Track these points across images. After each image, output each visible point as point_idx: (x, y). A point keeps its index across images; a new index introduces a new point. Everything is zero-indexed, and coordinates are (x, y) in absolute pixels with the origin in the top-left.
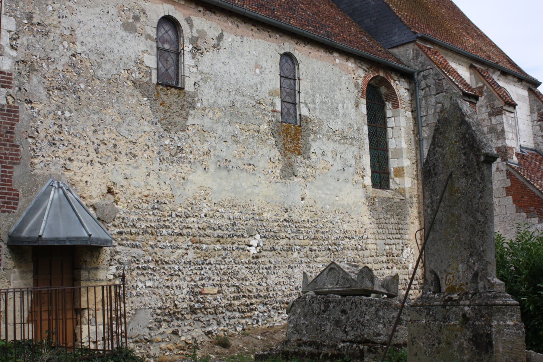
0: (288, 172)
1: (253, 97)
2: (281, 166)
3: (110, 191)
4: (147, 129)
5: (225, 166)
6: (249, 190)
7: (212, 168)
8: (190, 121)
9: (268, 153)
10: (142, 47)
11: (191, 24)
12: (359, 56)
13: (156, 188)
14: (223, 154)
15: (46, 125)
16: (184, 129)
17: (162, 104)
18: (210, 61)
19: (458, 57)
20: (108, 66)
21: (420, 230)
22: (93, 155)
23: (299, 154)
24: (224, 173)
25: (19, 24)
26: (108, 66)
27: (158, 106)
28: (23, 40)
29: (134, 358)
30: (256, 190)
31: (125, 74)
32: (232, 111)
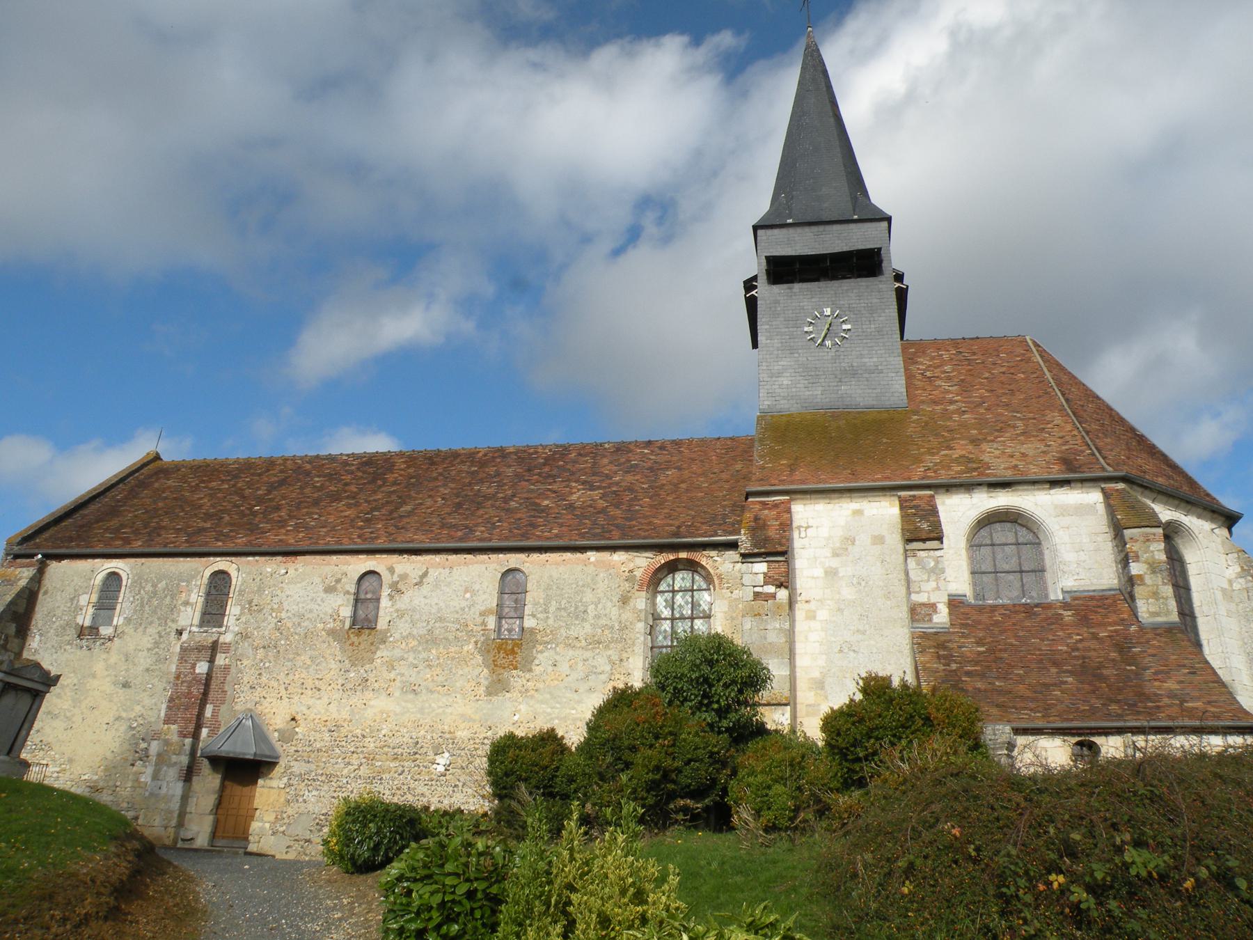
0: (491, 692)
1: (458, 621)
2: (486, 683)
3: (293, 719)
4: (333, 666)
5: (413, 690)
6: (440, 710)
7: (397, 694)
8: (379, 654)
9: (476, 671)
10: (340, 602)
11: (391, 570)
12: (1146, 488)
13: (335, 713)
14: (412, 679)
15: (248, 677)
16: (372, 661)
17: (352, 644)
18: (412, 598)
19: (1183, 505)
20: (306, 624)
21: (793, 731)
22: (283, 692)
23: (516, 668)
24: (411, 696)
25: (243, 608)
26: (306, 624)
27: (347, 647)
28: (243, 619)
29: (638, 694)
30: (449, 710)
31: (320, 626)
32: (430, 640)
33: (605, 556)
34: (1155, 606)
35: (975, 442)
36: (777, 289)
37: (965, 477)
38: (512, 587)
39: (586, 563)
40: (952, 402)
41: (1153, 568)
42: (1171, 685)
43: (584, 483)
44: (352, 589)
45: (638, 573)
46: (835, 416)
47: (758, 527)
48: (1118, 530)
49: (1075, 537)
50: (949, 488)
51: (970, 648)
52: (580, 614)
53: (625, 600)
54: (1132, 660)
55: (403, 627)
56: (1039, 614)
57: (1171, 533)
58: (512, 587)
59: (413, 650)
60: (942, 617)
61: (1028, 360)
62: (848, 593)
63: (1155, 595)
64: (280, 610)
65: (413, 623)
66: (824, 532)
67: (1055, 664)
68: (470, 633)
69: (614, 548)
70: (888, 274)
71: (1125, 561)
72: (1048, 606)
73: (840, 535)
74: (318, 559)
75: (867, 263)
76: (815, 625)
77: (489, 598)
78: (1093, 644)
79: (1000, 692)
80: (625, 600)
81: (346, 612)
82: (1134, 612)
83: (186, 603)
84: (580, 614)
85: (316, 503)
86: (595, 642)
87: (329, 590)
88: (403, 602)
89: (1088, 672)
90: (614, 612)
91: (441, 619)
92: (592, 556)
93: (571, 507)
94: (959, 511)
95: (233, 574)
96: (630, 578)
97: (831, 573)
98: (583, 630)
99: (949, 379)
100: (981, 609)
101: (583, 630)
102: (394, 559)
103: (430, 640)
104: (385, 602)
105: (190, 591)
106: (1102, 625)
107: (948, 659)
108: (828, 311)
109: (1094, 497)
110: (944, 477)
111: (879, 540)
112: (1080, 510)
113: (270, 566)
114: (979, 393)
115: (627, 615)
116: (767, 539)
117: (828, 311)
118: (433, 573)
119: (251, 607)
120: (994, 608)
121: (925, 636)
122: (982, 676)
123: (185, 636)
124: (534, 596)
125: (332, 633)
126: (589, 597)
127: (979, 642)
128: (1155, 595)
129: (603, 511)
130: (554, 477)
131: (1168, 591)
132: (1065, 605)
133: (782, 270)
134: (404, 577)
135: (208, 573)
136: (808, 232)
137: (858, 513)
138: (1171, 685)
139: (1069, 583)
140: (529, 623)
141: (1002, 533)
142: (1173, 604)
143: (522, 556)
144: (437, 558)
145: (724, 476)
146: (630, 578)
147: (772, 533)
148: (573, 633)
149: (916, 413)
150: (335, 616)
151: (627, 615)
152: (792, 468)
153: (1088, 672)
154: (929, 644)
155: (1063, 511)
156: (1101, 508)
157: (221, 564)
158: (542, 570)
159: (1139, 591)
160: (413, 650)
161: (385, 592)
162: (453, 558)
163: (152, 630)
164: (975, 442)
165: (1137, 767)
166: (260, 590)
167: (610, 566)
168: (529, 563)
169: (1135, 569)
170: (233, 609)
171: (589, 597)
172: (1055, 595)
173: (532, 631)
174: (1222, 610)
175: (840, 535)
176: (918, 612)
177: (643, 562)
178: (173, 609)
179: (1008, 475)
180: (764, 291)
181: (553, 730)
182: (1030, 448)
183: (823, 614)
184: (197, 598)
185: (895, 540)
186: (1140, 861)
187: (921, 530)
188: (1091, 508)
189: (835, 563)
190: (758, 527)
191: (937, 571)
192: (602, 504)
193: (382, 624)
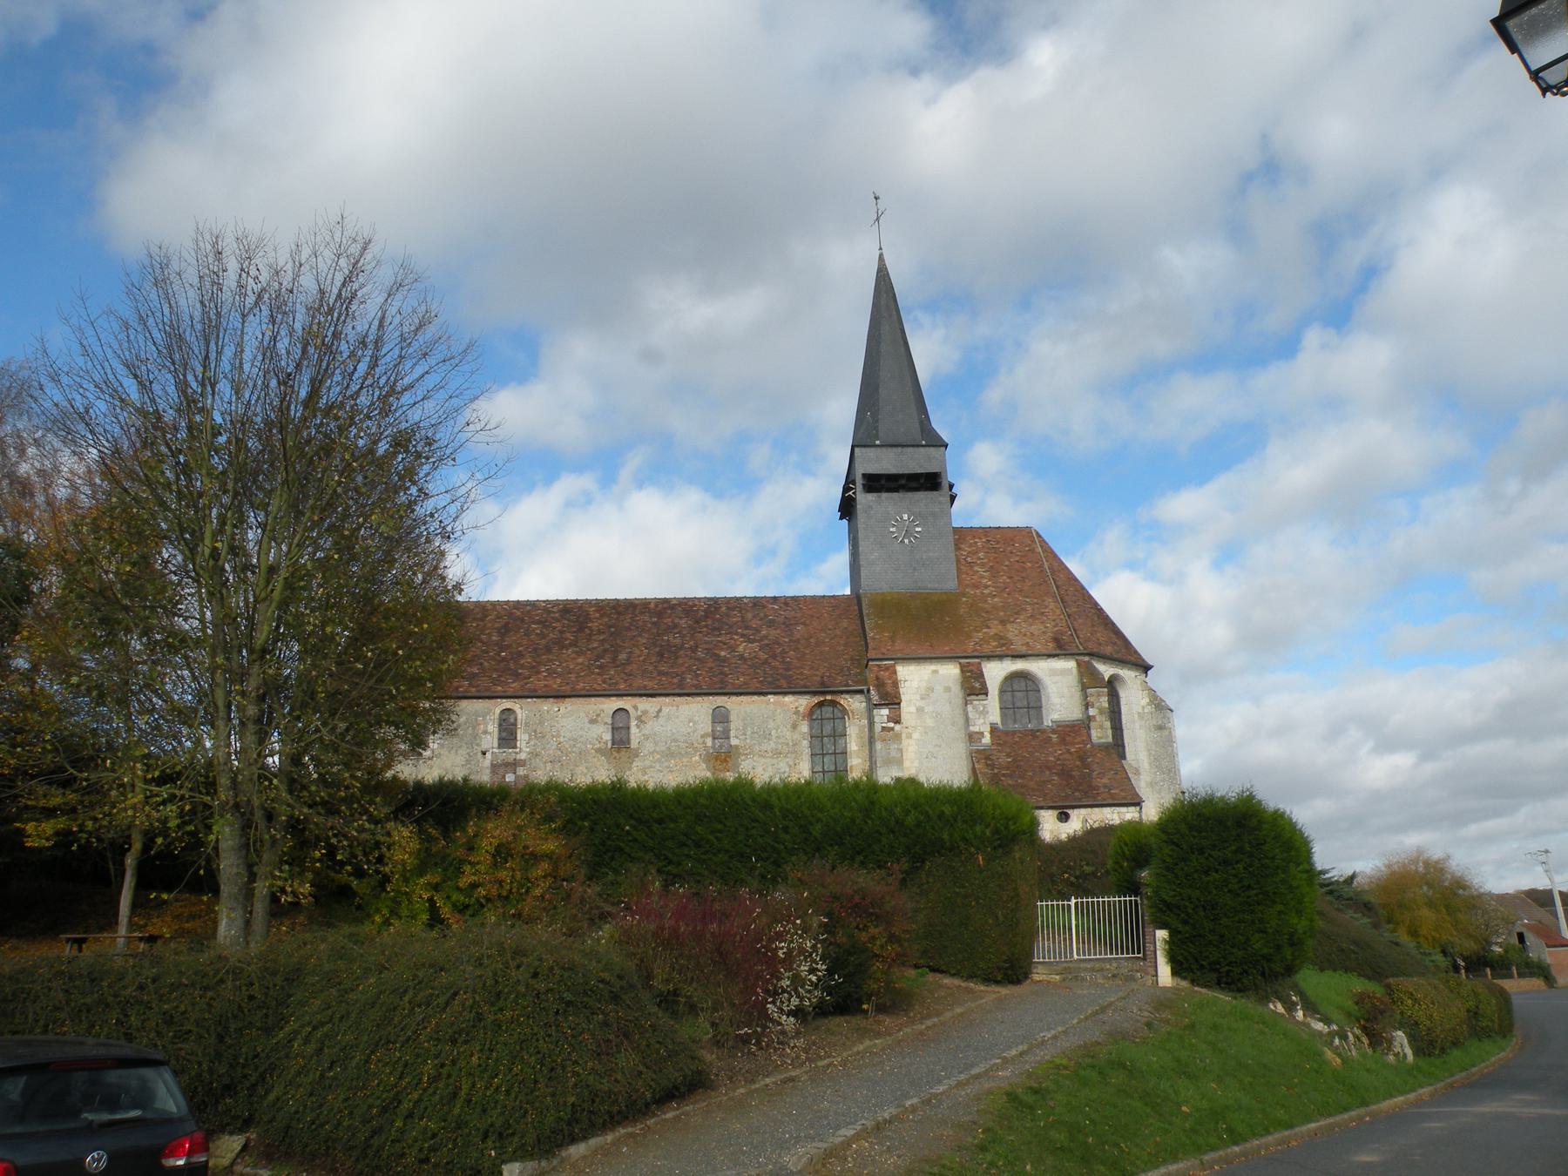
11: (636, 708)
18: (651, 726)
33: (780, 698)
34: (1101, 733)
35: (1003, 622)
36: (871, 497)
37: (999, 651)
38: (721, 718)
39: (768, 703)
40: (987, 587)
41: (1101, 712)
42: (1105, 781)
43: (743, 635)
44: (609, 721)
45: (801, 709)
46: (913, 596)
47: (880, 685)
48: (1084, 688)
49: (1059, 686)
50: (989, 657)
51: (1004, 760)
52: (767, 736)
53: (794, 727)
54: (1087, 766)
55: (649, 746)
56: (1038, 736)
57: (1112, 685)
58: (721, 718)
59: (658, 761)
60: (987, 739)
61: (1032, 551)
62: (930, 722)
63: (1101, 727)
64: (558, 736)
65: (656, 743)
66: (915, 684)
67: (1049, 769)
68: (696, 750)
69: (785, 694)
70: (945, 485)
71: (1087, 706)
72: (1043, 731)
73: (924, 684)
74: (582, 700)
75: (931, 482)
76: (912, 742)
77: (705, 725)
78: (1067, 756)
79: (1023, 786)
80: (794, 727)
81: (607, 737)
82: (1089, 736)
83: (485, 732)
84: (767, 736)
85: (548, 650)
86: (777, 754)
87: (592, 722)
88: (647, 729)
89: (1065, 774)
90: (788, 734)
91: (675, 741)
92: (772, 698)
93: (742, 657)
94: (995, 672)
95: (518, 711)
96: (797, 713)
97: (920, 710)
98: (769, 746)
99: (983, 565)
100: (1006, 733)
101: (769, 746)
102: (637, 699)
103: (670, 754)
104: (634, 730)
105: (486, 724)
106: (1073, 744)
107: (992, 767)
108: (905, 517)
109: (1071, 664)
110: (987, 649)
111: (948, 689)
112: (1063, 672)
113: (546, 706)
114: (1003, 579)
115: (796, 736)
116: (887, 694)
117: (905, 517)
118: (666, 710)
119: (536, 735)
120: (1014, 733)
121: (978, 751)
122: (1011, 776)
123: (488, 755)
124: (735, 724)
125: (598, 751)
126: (771, 724)
127: (1008, 755)
128: (1101, 727)
129: (766, 662)
130: (719, 629)
131: (1108, 724)
132: (1054, 731)
133: (876, 483)
134: (645, 712)
135: (498, 711)
136: (891, 452)
137: (936, 672)
138: (1105, 781)
139: (1055, 716)
140: (734, 742)
141: (1019, 685)
142: (1110, 732)
143: (725, 698)
144: (667, 700)
145: (838, 632)
146: (797, 713)
147: (889, 689)
148: (764, 747)
149: (964, 595)
150: (599, 740)
151: (796, 736)
152: (893, 639)
153: (1065, 774)
154: (980, 757)
155: (1054, 672)
156: (1075, 671)
157: (507, 704)
158: (741, 708)
159: (1093, 724)
160: (658, 761)
161: (633, 723)
162: (677, 699)
163: (463, 751)
164: (1003, 622)
165: (1077, 844)
166: (541, 723)
167: (783, 705)
168: (731, 703)
169: (1092, 712)
170: (522, 737)
171: (771, 724)
172: (1047, 723)
173: (737, 747)
174: (1137, 725)
175: (924, 684)
176: (973, 737)
177: (804, 702)
178: (475, 736)
179: (1023, 650)
180: (863, 499)
181: (451, 732)
182: (1036, 628)
183: (916, 735)
184: (493, 728)
185: (957, 690)
186: (1088, 869)
187: (973, 686)
188: (1070, 670)
189: (921, 704)
190: (880, 685)
191: (984, 713)
192: (763, 656)
193: (634, 744)
